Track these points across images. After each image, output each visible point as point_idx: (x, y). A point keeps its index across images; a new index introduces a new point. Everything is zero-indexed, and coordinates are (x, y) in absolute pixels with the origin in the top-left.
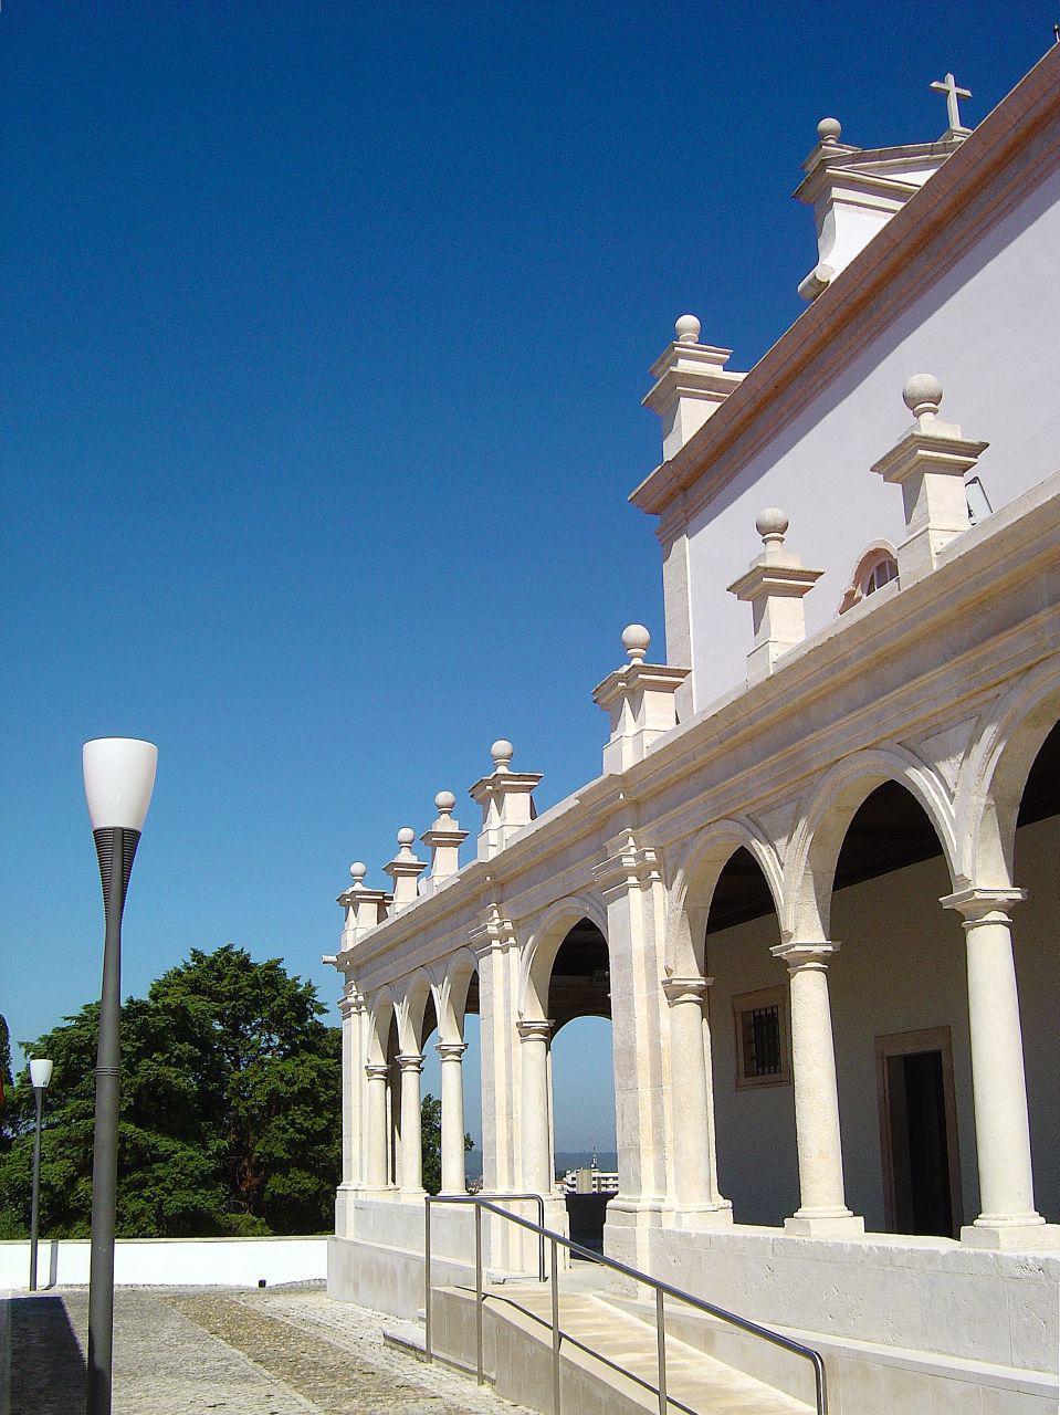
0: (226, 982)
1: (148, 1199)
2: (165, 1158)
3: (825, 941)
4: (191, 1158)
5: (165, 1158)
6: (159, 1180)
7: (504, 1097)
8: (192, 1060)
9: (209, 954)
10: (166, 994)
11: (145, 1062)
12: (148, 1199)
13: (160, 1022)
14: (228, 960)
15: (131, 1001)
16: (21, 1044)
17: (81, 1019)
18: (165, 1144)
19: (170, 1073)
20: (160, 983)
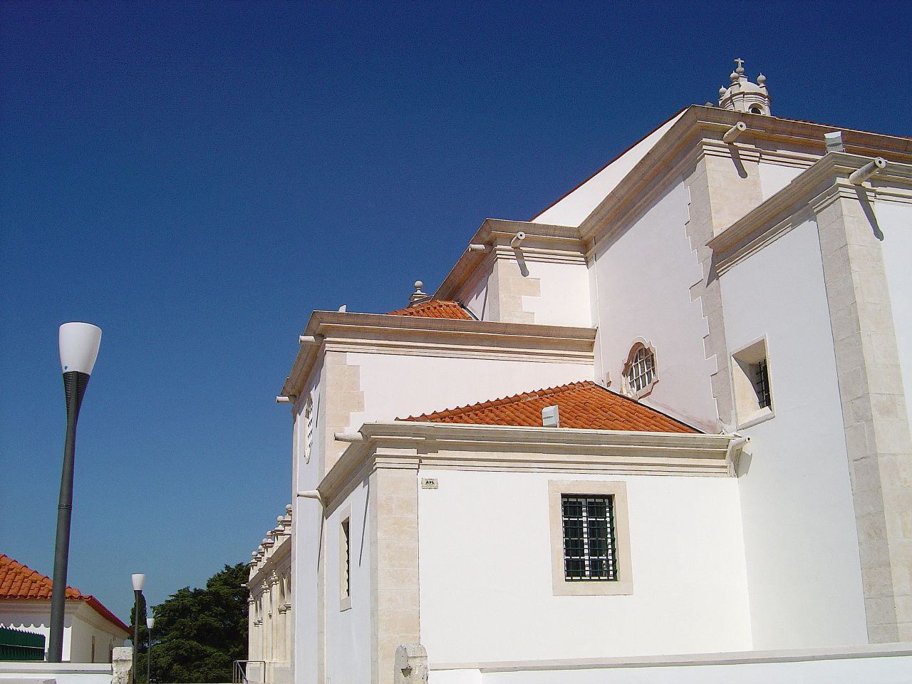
0: (239, 580)
1: (202, 673)
2: (209, 656)
3: (863, 645)
4: (220, 656)
5: (209, 656)
6: (206, 664)
7: (7, 668)
8: (221, 614)
9: (233, 567)
10: (213, 585)
11: (202, 615)
12: (202, 673)
13: (207, 598)
14: (241, 570)
15: (195, 590)
16: (151, 607)
17: (177, 596)
18: (209, 649)
19: (212, 620)
20: (211, 580)
